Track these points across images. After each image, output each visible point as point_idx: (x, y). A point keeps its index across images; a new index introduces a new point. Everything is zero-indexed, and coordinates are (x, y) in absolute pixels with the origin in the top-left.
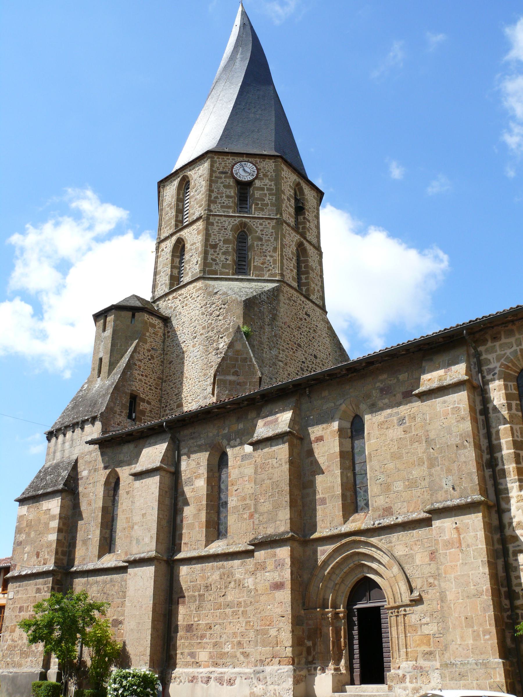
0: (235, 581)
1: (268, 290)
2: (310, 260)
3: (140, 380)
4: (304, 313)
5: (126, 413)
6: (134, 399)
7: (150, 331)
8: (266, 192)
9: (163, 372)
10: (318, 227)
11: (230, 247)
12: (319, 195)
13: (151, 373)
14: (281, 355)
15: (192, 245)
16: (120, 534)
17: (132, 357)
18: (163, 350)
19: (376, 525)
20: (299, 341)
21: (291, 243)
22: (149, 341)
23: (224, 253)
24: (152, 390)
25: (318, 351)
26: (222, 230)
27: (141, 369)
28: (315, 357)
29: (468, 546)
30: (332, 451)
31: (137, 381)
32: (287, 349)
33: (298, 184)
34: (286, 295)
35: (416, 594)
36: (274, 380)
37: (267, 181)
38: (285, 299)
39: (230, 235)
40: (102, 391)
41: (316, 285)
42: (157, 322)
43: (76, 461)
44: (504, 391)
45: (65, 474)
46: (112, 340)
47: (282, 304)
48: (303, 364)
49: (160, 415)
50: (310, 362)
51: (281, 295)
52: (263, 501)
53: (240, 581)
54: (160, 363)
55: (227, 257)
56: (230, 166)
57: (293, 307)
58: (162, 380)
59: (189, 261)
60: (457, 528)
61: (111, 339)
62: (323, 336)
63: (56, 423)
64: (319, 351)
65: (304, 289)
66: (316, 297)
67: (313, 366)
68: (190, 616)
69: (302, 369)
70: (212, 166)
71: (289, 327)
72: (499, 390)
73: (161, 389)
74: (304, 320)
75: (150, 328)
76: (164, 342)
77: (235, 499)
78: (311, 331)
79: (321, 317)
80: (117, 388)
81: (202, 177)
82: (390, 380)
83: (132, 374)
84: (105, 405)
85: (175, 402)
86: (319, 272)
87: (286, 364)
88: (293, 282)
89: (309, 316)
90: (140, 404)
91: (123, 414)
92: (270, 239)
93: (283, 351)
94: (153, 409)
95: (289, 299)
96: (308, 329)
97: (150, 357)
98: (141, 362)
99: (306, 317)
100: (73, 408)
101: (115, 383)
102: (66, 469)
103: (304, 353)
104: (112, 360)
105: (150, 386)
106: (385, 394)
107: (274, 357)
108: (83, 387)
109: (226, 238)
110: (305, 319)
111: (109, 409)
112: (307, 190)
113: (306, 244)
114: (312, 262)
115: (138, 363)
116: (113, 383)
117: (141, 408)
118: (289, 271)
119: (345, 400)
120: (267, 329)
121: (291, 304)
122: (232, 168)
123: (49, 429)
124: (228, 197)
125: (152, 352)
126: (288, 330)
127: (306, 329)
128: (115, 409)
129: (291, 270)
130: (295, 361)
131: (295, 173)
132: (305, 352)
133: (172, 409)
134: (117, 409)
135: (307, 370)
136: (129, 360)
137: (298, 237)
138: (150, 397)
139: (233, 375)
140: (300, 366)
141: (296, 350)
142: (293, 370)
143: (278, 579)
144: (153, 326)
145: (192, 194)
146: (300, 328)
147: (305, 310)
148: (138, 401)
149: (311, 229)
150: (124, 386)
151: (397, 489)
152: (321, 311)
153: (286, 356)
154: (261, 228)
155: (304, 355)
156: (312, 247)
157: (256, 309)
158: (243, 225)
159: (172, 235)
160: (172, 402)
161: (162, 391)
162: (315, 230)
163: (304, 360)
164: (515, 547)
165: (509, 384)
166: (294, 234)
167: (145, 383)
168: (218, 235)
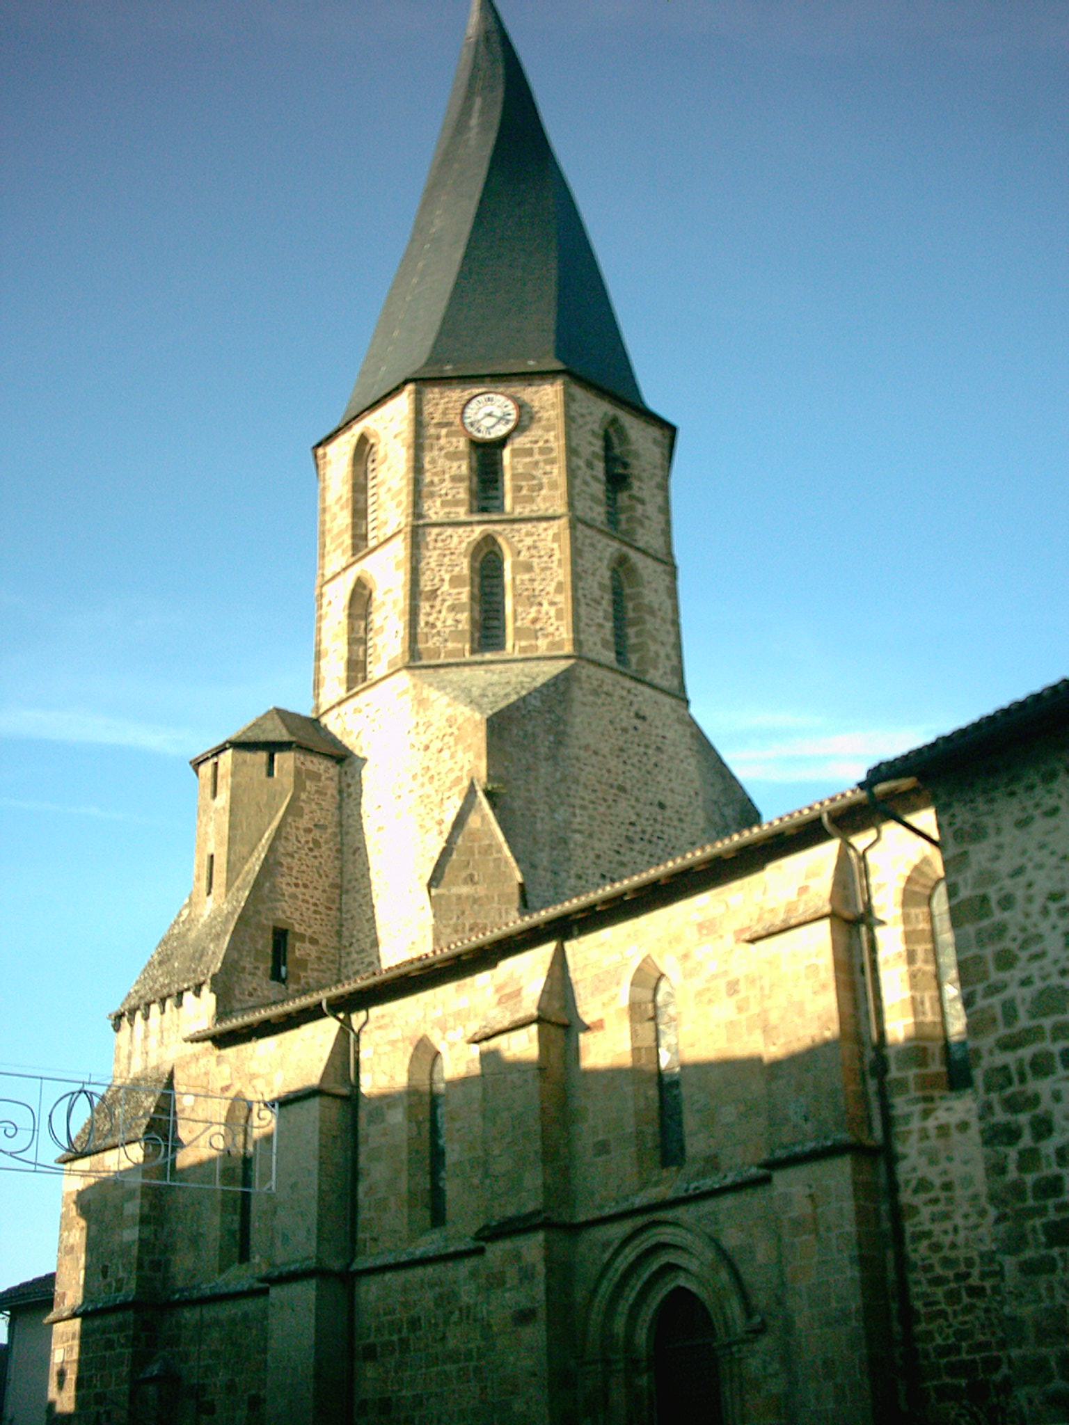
0: (461, 1310)
1: (544, 685)
2: (646, 592)
3: (293, 896)
4: (632, 714)
5: (266, 970)
6: (281, 937)
7: (308, 788)
8: (537, 457)
9: (341, 873)
10: (665, 510)
11: (464, 594)
13: (316, 876)
14: (578, 819)
16: (257, 1224)
17: (272, 849)
18: (340, 825)
19: (691, 1192)
20: (621, 778)
22: (306, 810)
23: (453, 608)
24: (320, 913)
26: (445, 556)
27: (294, 873)
28: (662, 806)
29: (828, 1229)
31: (287, 898)
33: (614, 421)
34: (586, 686)
35: (757, 1319)
36: (563, 875)
37: (540, 432)
39: (464, 566)
40: (215, 927)
42: (322, 767)
43: (171, 1075)
45: (149, 1103)
46: (231, 815)
47: (576, 707)
48: (632, 829)
49: (340, 964)
50: (647, 819)
51: (575, 687)
53: (468, 1307)
54: (334, 854)
56: (459, 406)
57: (605, 708)
60: (811, 1196)
61: (228, 814)
62: (681, 756)
63: (129, 995)
64: (672, 791)
65: (634, 658)
66: (661, 672)
67: (658, 827)
68: (385, 1383)
69: (629, 840)
71: (596, 753)
73: (340, 910)
74: (632, 732)
75: (308, 783)
76: (340, 808)
79: (673, 716)
80: (243, 920)
83: (274, 886)
84: (221, 957)
85: (367, 936)
86: (670, 611)
87: (591, 836)
89: (644, 718)
93: (583, 807)
94: (323, 952)
95: (595, 692)
96: (642, 749)
97: (311, 845)
98: (293, 857)
99: (637, 722)
101: (239, 910)
102: (152, 1092)
103: (633, 802)
104: (233, 858)
105: (315, 905)
106: (707, 935)
107: (562, 825)
108: (180, 915)
109: (455, 573)
110: (635, 728)
111: (230, 966)
112: (636, 430)
113: (634, 556)
114: (652, 595)
115: (286, 861)
116: (235, 909)
117: (297, 953)
118: (593, 629)
120: (544, 769)
121: (599, 702)
122: (463, 413)
123: (116, 1007)
125: (316, 834)
126: (594, 760)
127: (637, 749)
129: (600, 626)
132: (637, 800)
133: (363, 951)
134: (247, 963)
136: (266, 858)
137: (616, 545)
139: (465, 882)
140: (625, 833)
142: (605, 845)
143: (525, 1304)
144: (316, 777)
146: (622, 750)
147: (634, 709)
149: (648, 518)
150: (258, 912)
152: (674, 702)
153: (591, 817)
154: (529, 541)
155: (633, 807)
156: (649, 561)
158: (489, 540)
160: (361, 936)
161: (341, 912)
163: (634, 818)
164: (916, 1226)
166: (605, 541)
168: (438, 568)
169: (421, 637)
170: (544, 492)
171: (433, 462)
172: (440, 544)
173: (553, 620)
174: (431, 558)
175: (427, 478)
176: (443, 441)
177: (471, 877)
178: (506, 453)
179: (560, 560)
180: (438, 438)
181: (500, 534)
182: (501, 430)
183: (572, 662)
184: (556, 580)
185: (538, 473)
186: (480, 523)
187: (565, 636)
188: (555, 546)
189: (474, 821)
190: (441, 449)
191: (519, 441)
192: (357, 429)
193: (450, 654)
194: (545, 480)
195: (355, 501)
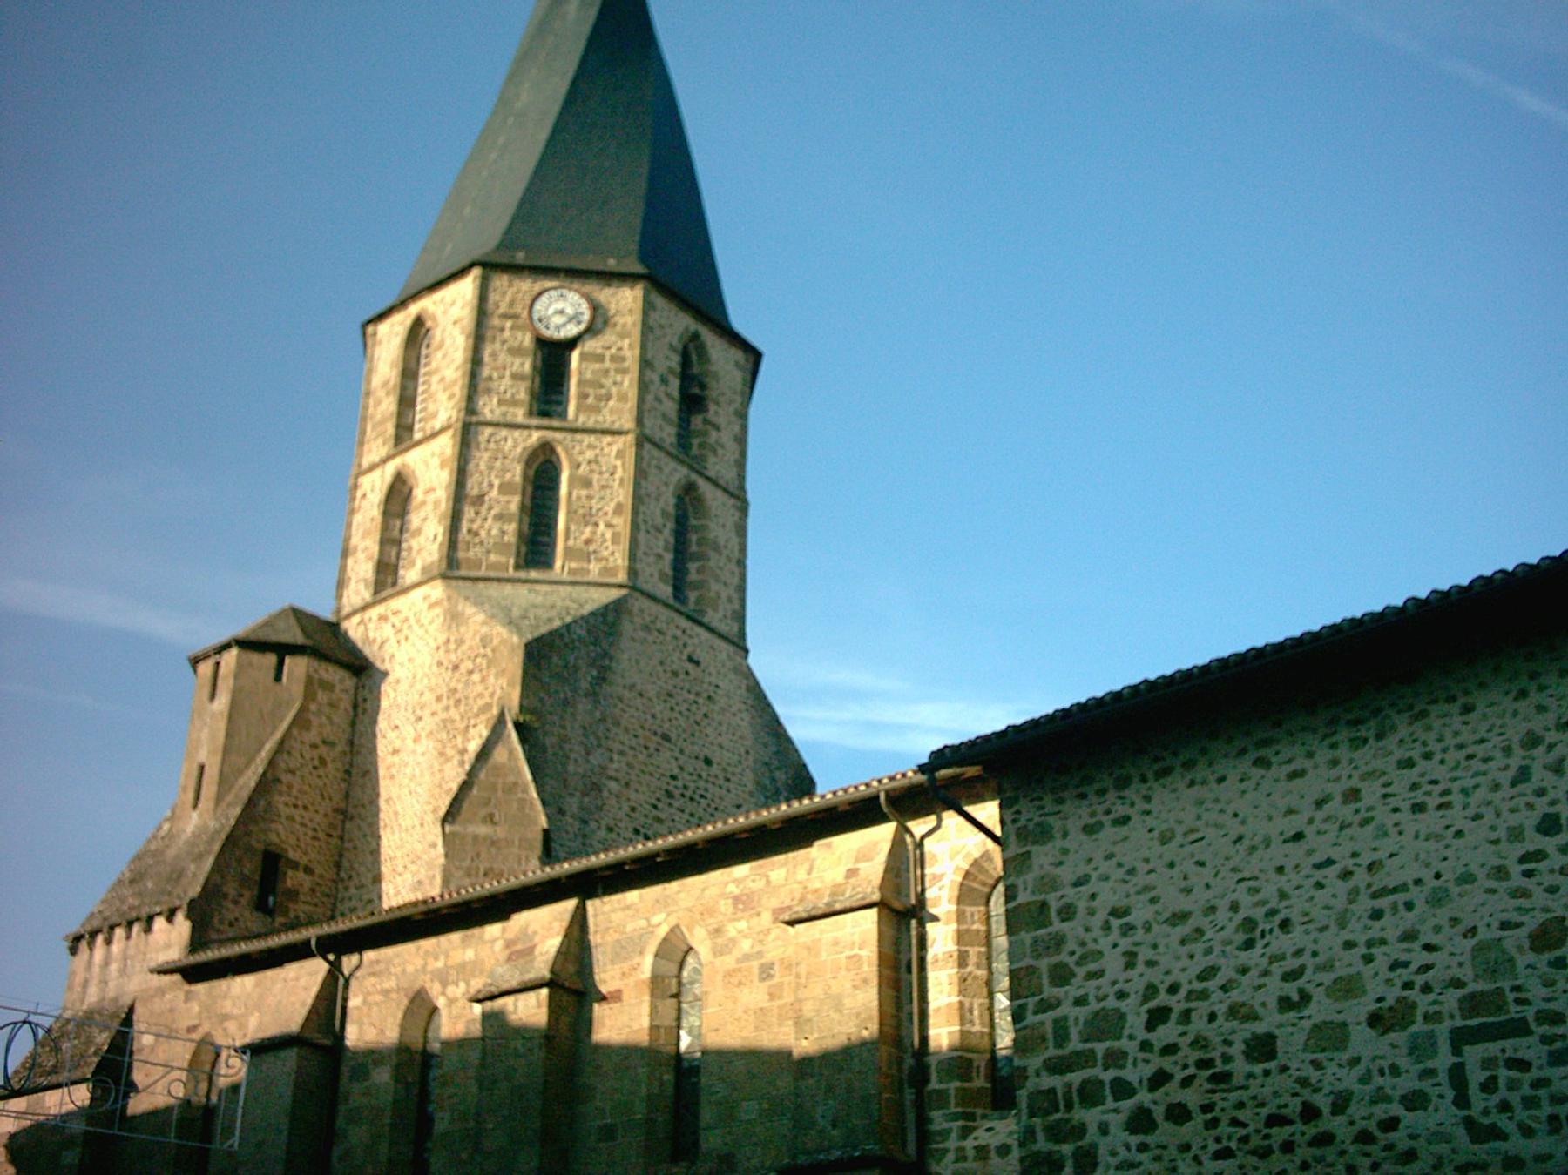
2: (712, 525)
4: (685, 657)
8: (607, 364)
10: (742, 440)
12: (752, 359)
14: (615, 766)
15: (427, 492)
17: (272, 763)
18: (351, 743)
20: (667, 725)
21: (663, 489)
23: (499, 517)
25: (716, 748)
27: (294, 792)
28: (708, 762)
30: (636, 1027)
32: (632, 748)
33: (695, 337)
34: (637, 619)
37: (614, 338)
38: (635, 630)
39: (516, 473)
41: (725, 584)
43: (131, 1010)
44: (954, 926)
45: (103, 1039)
48: (673, 783)
50: (691, 774)
52: (491, 1126)
55: (506, 527)
58: (344, 814)
59: (419, 531)
62: (734, 709)
63: (92, 915)
64: (721, 746)
66: (721, 614)
70: (483, 298)
71: (641, 695)
72: (947, 923)
73: (341, 838)
74: (682, 676)
76: (353, 724)
77: (447, 1116)
78: (701, 701)
79: (729, 664)
80: (231, 841)
81: (458, 325)
82: (753, 881)
88: (661, 585)
89: (697, 663)
90: (285, 874)
91: (244, 901)
92: (611, 483)
93: (622, 753)
95: (647, 628)
96: (692, 697)
97: (316, 763)
99: (690, 667)
100: (132, 882)
101: (228, 829)
102: (105, 1028)
103: (677, 754)
105: (315, 830)
106: (743, 910)
110: (687, 673)
114: (718, 528)
115: (286, 778)
119: (668, 915)
120: (583, 706)
121: (650, 639)
122: (532, 306)
124: (515, 377)
127: (686, 695)
128: (225, 889)
129: (660, 556)
130: (651, 775)
131: (685, 311)
132: (682, 751)
134: (231, 889)
135: (683, 795)
137: (684, 471)
138: (313, 856)
139: (484, 821)
141: (657, 750)
145: (434, 365)
148: (282, 865)
149: (722, 447)
151: (748, 1117)
152: (731, 648)
153: (629, 765)
154: (589, 454)
156: (719, 493)
157: (555, 659)
158: (546, 449)
159: (384, 461)
162: (732, 446)
163: (676, 771)
165: (969, 909)
166: (672, 464)
167: (303, 825)
169: (461, 545)
170: (611, 403)
171: (494, 355)
172: (492, 446)
173: (609, 543)
174: (481, 460)
175: (486, 372)
176: (507, 334)
177: (491, 816)
178: (575, 356)
179: (622, 480)
180: (502, 329)
181: (559, 442)
182: (572, 330)
183: (624, 592)
184: (616, 500)
185: (607, 382)
186: (538, 428)
187: (620, 562)
188: (619, 463)
189: (499, 755)
190: (504, 342)
191: (590, 345)
192: (414, 309)
193: (491, 566)
194: (614, 390)
195: (403, 388)
